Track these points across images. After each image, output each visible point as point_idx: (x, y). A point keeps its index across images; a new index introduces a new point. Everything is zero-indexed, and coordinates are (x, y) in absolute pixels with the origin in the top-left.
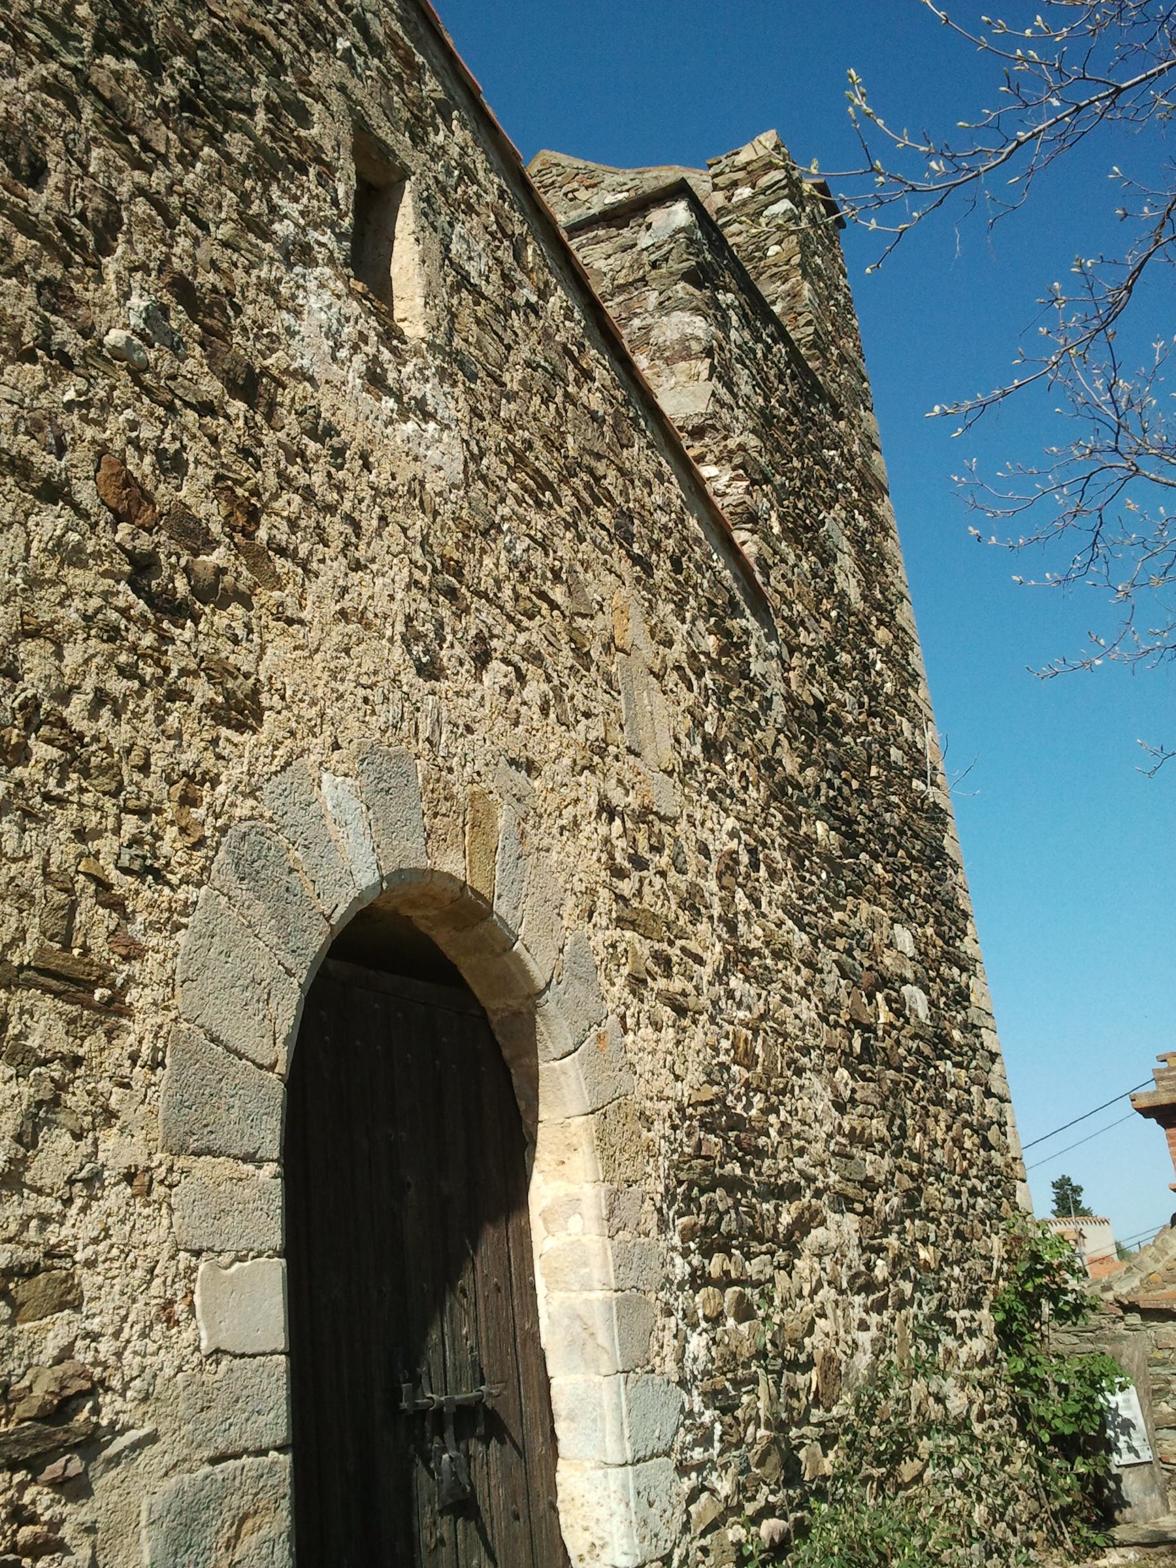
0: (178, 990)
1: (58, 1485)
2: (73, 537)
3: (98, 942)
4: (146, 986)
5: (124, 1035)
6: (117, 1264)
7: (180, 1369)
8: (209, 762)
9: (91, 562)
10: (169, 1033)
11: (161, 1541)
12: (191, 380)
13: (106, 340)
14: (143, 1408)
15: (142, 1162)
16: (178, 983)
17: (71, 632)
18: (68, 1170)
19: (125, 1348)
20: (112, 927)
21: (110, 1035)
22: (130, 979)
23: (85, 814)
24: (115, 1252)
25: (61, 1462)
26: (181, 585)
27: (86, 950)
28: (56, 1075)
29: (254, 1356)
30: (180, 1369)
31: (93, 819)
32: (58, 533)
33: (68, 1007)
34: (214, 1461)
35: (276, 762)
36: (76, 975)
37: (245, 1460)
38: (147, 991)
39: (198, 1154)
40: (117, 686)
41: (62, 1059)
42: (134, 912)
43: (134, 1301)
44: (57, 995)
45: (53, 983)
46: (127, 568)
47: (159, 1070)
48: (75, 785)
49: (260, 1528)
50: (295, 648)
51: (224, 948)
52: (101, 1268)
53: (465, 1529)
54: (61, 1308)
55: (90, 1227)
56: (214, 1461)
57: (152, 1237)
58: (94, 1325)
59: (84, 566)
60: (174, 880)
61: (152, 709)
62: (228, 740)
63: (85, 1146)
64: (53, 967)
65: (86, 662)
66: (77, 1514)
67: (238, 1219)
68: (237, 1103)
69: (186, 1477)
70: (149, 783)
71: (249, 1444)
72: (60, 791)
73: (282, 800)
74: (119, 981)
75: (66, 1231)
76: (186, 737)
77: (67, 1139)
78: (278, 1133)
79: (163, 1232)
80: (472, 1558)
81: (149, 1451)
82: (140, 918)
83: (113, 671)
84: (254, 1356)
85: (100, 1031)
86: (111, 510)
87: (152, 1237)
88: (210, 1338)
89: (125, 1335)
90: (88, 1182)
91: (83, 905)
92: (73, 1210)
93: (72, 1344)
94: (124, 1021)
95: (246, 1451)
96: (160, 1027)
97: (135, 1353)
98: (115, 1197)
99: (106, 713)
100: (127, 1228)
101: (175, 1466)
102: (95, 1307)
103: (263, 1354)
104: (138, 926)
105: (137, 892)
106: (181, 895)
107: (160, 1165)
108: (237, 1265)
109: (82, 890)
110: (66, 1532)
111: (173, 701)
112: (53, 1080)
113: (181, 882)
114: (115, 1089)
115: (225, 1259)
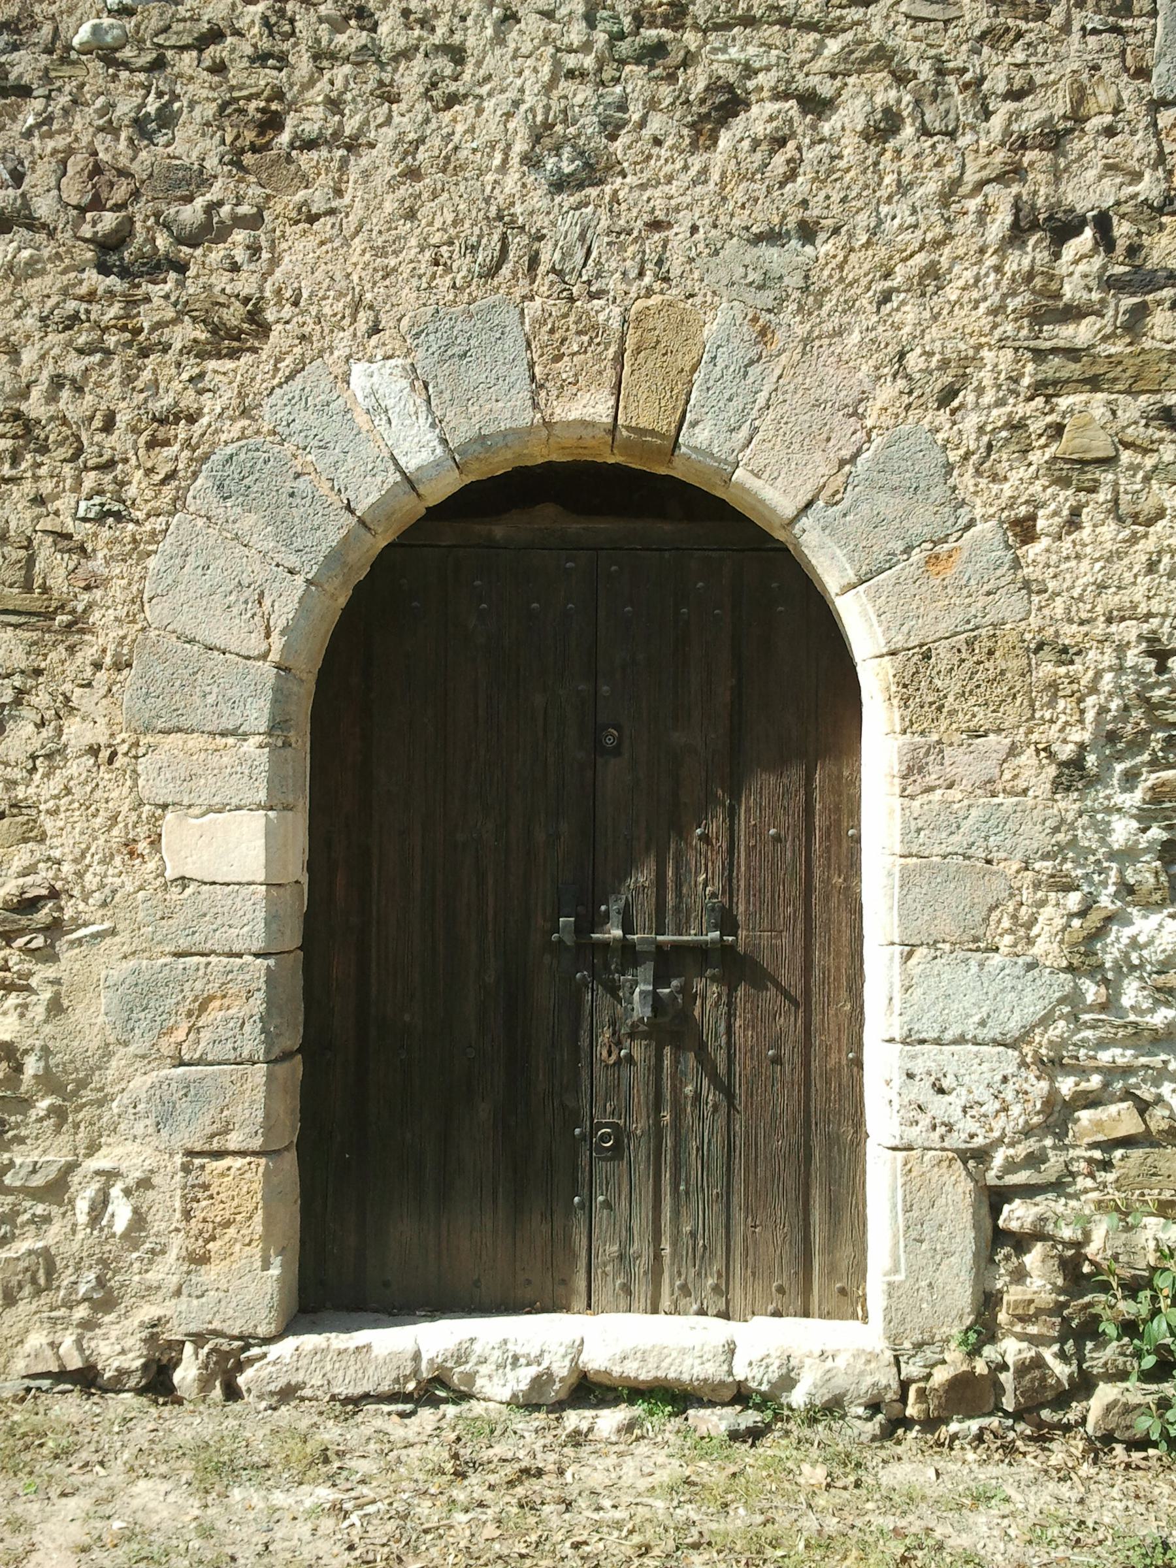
0: (147, 606)
1: (26, 951)
2: (26, 254)
3: (58, 582)
4: (108, 608)
5: (86, 648)
6: (77, 813)
7: (141, 888)
8: (189, 400)
9: (49, 266)
10: (134, 641)
11: (115, 1001)
12: (191, 19)
13: (76, 42)
14: (100, 912)
15: (103, 740)
16: (145, 599)
17: (28, 337)
18: (30, 749)
19: (86, 871)
20: (71, 567)
21: (71, 649)
22: (89, 607)
23: (41, 484)
24: (76, 805)
25: (27, 938)
26: (162, 241)
27: (45, 589)
28: (17, 684)
29: (228, 885)
30: (141, 888)
31: (47, 487)
32: (9, 257)
33: (28, 634)
34: (178, 955)
35: (280, 374)
36: (34, 610)
37: (213, 959)
38: (111, 611)
39: (168, 732)
40: (74, 366)
41: (22, 672)
42: (94, 550)
43: (95, 839)
44: (16, 626)
45: (13, 619)
46: (89, 255)
47: (125, 672)
48: (30, 461)
49: (228, 1008)
50: (322, 243)
51: (201, 562)
52: (62, 816)
53: (676, 1062)
54: (25, 840)
55: (55, 785)
56: (178, 955)
57: (114, 794)
58: (56, 854)
59: (43, 272)
60: (140, 515)
61: (118, 373)
62: (215, 372)
63: (48, 732)
64: (11, 608)
65: (42, 357)
66: (42, 972)
67: (211, 780)
68: (215, 690)
69: (145, 962)
70: (112, 440)
71: (215, 947)
72: (14, 472)
73: (288, 409)
74: (80, 608)
75: (31, 790)
76: (163, 384)
77: (31, 728)
78: (266, 711)
79: (125, 790)
80: (683, 1084)
81: (108, 940)
82: (100, 555)
83: (73, 354)
84: (228, 885)
85: (61, 648)
86: (75, 207)
87: (114, 794)
88: (173, 868)
89: (87, 861)
90: (49, 756)
91: (42, 555)
92: (37, 777)
93: (36, 864)
94: (87, 637)
95: (213, 952)
96: (124, 637)
97: (95, 875)
98: (77, 767)
99: (65, 394)
100: (88, 789)
101: (133, 953)
102: (56, 842)
103: (239, 884)
104: (100, 561)
105: (95, 535)
106: (148, 527)
107: (123, 741)
108: (212, 815)
109: (40, 544)
110: (34, 982)
111: (147, 356)
112: (15, 688)
113: (148, 516)
114: (77, 690)
115: (196, 811)
